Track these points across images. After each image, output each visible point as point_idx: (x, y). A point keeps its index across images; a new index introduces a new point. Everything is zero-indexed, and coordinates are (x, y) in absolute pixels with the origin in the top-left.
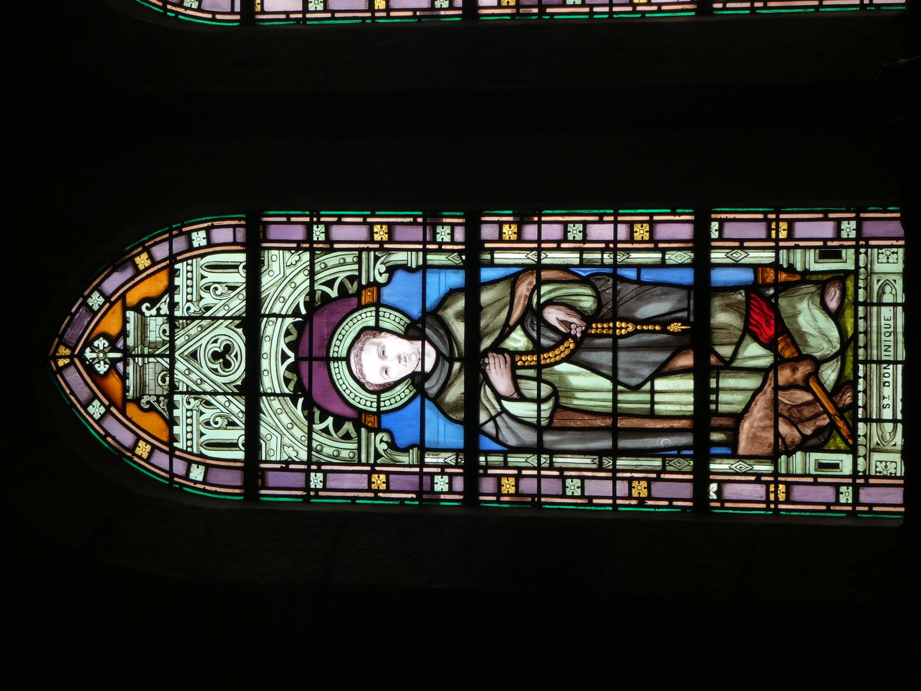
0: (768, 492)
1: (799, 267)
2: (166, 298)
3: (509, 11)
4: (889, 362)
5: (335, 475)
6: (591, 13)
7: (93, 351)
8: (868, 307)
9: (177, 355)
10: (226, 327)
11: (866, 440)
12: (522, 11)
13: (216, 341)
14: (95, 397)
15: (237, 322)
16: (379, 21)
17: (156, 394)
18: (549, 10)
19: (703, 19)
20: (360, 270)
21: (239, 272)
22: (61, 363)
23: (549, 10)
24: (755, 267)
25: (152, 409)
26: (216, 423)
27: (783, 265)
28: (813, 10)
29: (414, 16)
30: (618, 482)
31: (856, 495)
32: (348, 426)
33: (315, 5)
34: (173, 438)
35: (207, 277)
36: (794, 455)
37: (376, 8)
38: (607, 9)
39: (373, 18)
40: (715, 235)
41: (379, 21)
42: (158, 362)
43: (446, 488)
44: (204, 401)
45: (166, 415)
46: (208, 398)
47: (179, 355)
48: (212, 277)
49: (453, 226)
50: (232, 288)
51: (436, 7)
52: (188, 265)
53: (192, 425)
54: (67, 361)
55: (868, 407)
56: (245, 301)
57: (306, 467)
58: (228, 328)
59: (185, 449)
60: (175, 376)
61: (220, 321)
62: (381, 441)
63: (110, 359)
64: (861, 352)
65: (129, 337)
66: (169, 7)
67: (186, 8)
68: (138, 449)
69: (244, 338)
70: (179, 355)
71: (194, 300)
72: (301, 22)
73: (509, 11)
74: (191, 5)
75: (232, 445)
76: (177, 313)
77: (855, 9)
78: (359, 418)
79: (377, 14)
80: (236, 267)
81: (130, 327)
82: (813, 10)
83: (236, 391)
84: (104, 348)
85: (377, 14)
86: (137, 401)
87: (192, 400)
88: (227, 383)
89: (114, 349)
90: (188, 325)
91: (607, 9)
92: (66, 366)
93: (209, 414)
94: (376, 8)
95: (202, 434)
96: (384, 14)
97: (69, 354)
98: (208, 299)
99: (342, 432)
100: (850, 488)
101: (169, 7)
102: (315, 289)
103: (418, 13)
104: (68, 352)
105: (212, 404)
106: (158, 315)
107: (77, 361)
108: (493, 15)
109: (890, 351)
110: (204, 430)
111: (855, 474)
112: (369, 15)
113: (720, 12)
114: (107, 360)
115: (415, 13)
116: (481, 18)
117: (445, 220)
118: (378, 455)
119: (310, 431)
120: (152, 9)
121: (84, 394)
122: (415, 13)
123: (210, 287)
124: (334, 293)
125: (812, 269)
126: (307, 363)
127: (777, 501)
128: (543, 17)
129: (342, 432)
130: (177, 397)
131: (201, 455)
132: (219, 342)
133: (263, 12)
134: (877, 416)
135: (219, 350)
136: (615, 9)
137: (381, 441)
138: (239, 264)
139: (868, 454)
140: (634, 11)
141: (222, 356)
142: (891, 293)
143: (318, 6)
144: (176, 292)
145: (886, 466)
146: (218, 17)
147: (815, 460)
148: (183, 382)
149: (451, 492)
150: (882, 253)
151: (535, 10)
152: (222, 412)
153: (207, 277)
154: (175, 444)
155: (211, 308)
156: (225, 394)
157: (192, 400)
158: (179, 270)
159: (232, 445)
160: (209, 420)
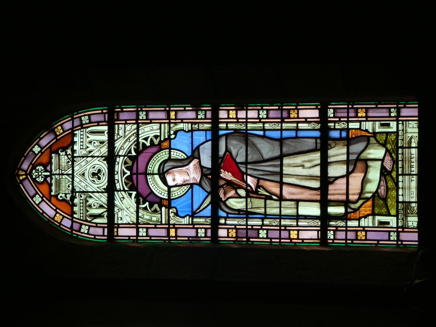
3: (232, 239)
6: (271, 242)
8: (404, 176)
9: (75, 174)
10: (98, 161)
11: (403, 142)
12: (238, 239)
13: (94, 168)
14: (37, 193)
15: (103, 158)
16: (172, 241)
18: (251, 240)
19: (323, 249)
20: (160, 132)
21: (105, 135)
22: (21, 178)
23: (251, 240)
26: (94, 206)
28: (374, 245)
29: (189, 240)
30: (348, 233)
31: (398, 236)
32: (156, 206)
33: (142, 233)
34: (73, 213)
35: (89, 147)
37: (171, 235)
38: (278, 240)
39: (169, 240)
41: (172, 241)
43: (203, 235)
44: (89, 195)
46: (91, 194)
47: (76, 174)
48: (92, 137)
49: (206, 111)
50: (102, 143)
51: (199, 236)
52: (81, 131)
53: (83, 138)
54: (24, 177)
56: (107, 149)
57: (136, 109)
58: (99, 161)
59: (79, 218)
60: (74, 184)
61: (96, 158)
64: (400, 170)
65: (53, 179)
66: (74, 232)
67: (82, 233)
69: (107, 165)
70: (76, 174)
71: (84, 148)
72: (136, 241)
73: (232, 239)
74: (84, 231)
76: (75, 155)
77: (394, 246)
78: (160, 202)
79: (171, 238)
80: (103, 132)
81: (53, 160)
82: (374, 245)
83: (103, 191)
84: (41, 170)
85: (171, 238)
87: (82, 195)
88: (99, 187)
89: (46, 171)
90: (80, 160)
91: (278, 240)
92: (24, 179)
94: (171, 235)
96: (174, 239)
98: (91, 147)
99: (153, 209)
100: (396, 233)
101: (74, 232)
102: (139, 141)
103: (190, 239)
104: (24, 173)
105: (92, 197)
108: (225, 241)
111: (398, 227)
112: (167, 238)
113: (331, 244)
115: (189, 239)
116: (220, 242)
117: (202, 108)
119: (138, 208)
120: (66, 232)
121: (32, 192)
122: (189, 239)
123: (92, 142)
124: (148, 144)
128: (248, 243)
129: (153, 209)
132: (95, 168)
133: (118, 236)
135: (95, 172)
136: (282, 241)
138: (104, 131)
140: (291, 242)
141: (96, 175)
142: (414, 142)
143: (143, 234)
144: (75, 144)
146: (97, 237)
147: (379, 128)
148: (78, 187)
149: (206, 236)
150: (411, 124)
151: (245, 239)
152: (97, 200)
153: (89, 147)
154: (75, 216)
155: (92, 151)
156: (98, 192)
157: (82, 195)
158: (77, 134)
159: (100, 216)
160: (91, 204)
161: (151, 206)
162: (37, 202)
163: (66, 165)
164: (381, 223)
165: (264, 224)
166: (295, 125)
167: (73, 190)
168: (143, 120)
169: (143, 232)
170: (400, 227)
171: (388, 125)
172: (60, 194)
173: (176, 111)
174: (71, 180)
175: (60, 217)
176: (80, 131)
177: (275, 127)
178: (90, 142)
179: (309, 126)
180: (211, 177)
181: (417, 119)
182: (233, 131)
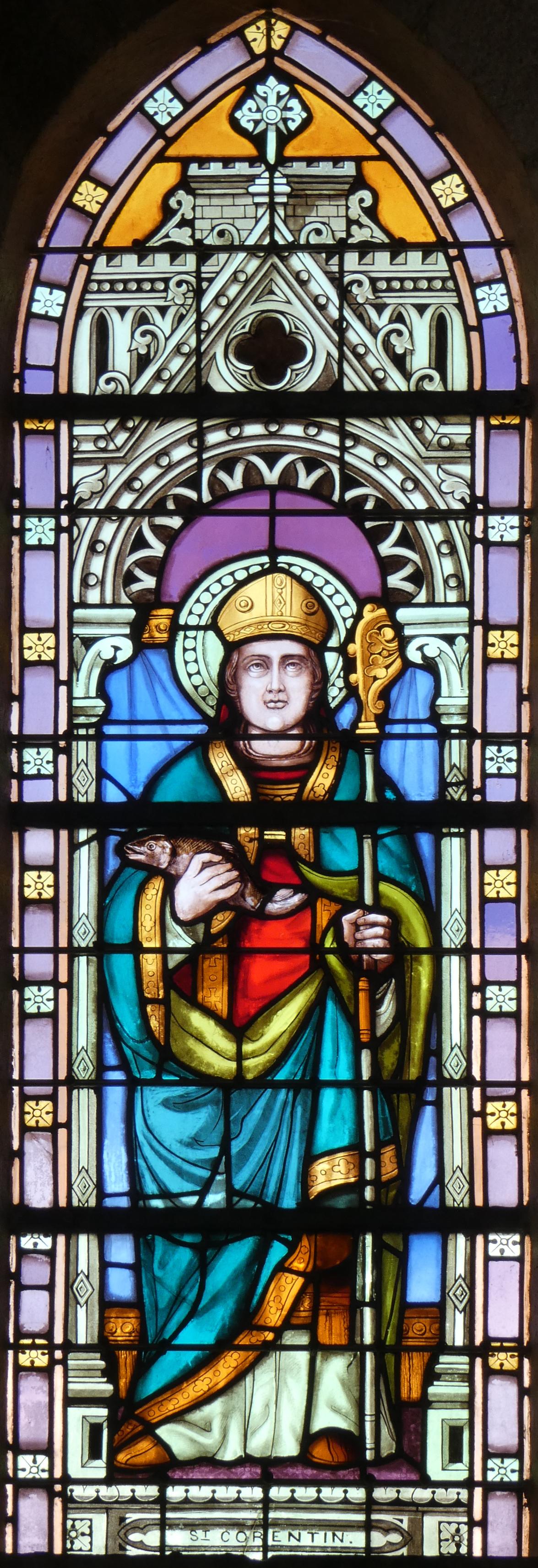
0: (33, 1336)
4: (265, 1540)
5: (53, 465)
25: (167, 212)
27: (439, 1363)
30: (50, 957)
34: (113, 253)
45: (155, 242)
54: (259, 47)
55: (187, 1506)
62: (117, 649)
63: (264, 133)
68: (91, 186)
75: (101, 364)
86: (185, 183)
89: (284, 139)
93: (164, 324)
95: (122, 311)
97: (273, 46)
100: (45, 1475)
104: (277, 44)
106: (350, 222)
107: (260, 64)
109: (289, 1540)
110: (130, 315)
114: (261, 127)
118: (88, 642)
123: (403, 322)
127: (19, 1349)
130: (191, 260)
131: (81, 311)
137: (117, 649)
143: (494, 1001)
145: (83, 1534)
154: (102, 260)
159: (101, 364)
161: (146, 565)
165: (76, 959)
167: (203, 252)
168: (486, 644)
169: (39, 999)
171: (455, 1456)
172: (191, 198)
173: (517, 1374)
174: (251, 241)
176: (448, 274)
177: (454, 1298)
178: (399, 318)
179: (454, 1172)
181: (479, 1202)
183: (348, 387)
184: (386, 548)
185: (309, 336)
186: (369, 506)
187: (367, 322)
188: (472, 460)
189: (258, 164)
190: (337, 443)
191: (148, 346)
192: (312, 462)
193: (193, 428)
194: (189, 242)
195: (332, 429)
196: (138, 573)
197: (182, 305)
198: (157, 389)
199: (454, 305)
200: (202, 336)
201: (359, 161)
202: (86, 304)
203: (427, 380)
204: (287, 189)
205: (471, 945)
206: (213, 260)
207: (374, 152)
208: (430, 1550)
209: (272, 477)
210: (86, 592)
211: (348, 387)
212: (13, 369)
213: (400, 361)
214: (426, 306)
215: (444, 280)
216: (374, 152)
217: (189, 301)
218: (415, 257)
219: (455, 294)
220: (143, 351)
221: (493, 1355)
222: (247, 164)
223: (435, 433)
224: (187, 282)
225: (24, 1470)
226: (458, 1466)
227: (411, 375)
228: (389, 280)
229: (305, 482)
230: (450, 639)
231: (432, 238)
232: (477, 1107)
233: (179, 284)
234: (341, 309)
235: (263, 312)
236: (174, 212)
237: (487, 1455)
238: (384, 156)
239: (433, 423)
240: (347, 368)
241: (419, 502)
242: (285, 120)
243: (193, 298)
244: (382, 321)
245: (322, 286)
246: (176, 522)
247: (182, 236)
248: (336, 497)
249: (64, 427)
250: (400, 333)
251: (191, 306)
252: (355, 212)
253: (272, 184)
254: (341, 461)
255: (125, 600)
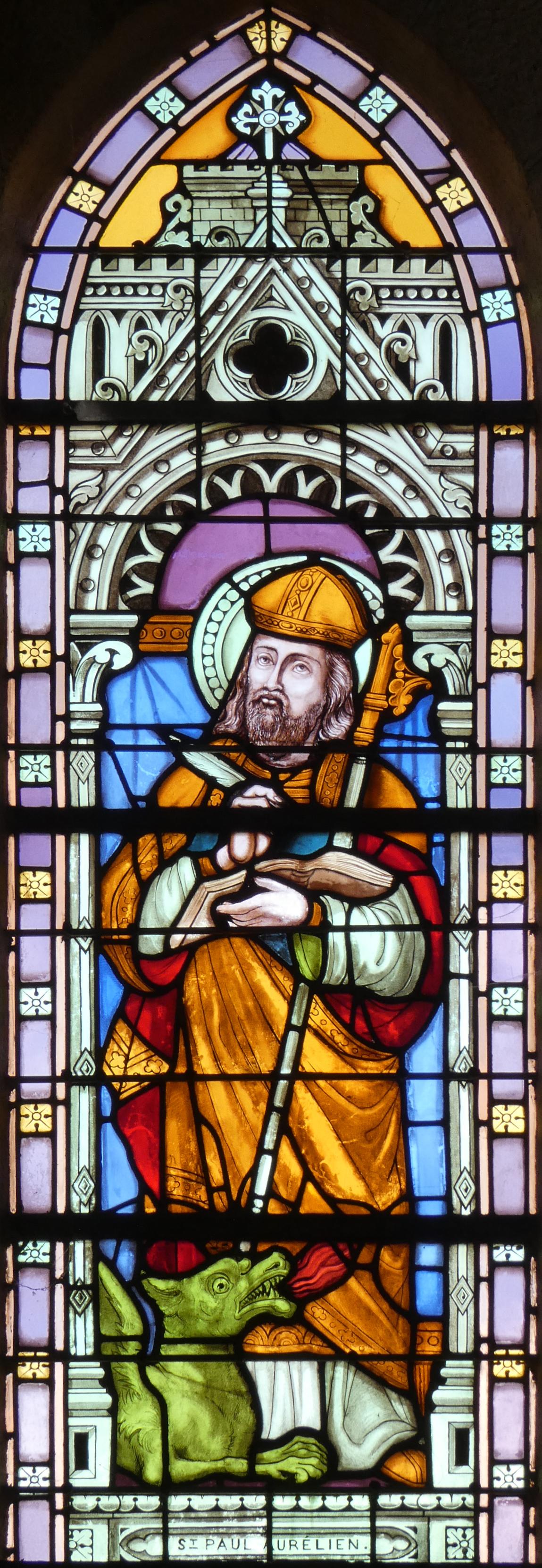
1: (438, 1395)
2: (383, 242)
7: (276, 100)
14: (190, 104)
17: (194, 223)
24: (443, 1320)
25: (167, 217)
31: (36, 1494)
36: (104, 1390)
40: (500, 1255)
42: (256, 226)
54: (260, 47)
59: (90, 280)
62: (113, 652)
89: (281, 140)
97: (274, 48)
100: (46, 1484)
104: (278, 46)
107: (262, 64)
111: (69, 1491)
125: (434, 1418)
126: (261, 514)
130: (189, 264)
131: (77, 314)
134: (174, 1528)
137: (113, 652)
139: (101, 1515)
147: (449, 1423)
150: (464, 1536)
154: (97, 263)
161: (144, 571)
162: (151, 105)
163: (309, 225)
164: (82, 1440)
166: (465, 969)
170: (67, 1500)
171: (461, 1458)
172: (188, 201)
175: (90, 203)
176: (452, 283)
179: (460, 1052)
180: (10, 1562)
182: (442, 883)
183: (350, 396)
184: (387, 555)
185: (310, 345)
186: (371, 513)
187: (370, 330)
188: (475, 470)
189: (257, 167)
190: (338, 452)
191: (147, 353)
192: (312, 469)
193: (193, 434)
194: (187, 245)
195: (332, 437)
196: (135, 579)
197: (181, 311)
198: (156, 396)
199: (460, 314)
200: (202, 342)
201: (362, 165)
202: (82, 307)
203: (431, 391)
204: (287, 193)
205: (478, 1070)
206: (212, 265)
207: (378, 156)
208: (437, 1556)
209: (271, 485)
210: (84, 597)
211: (350, 396)
212: (6, 1352)
213: (402, 370)
214: (429, 315)
215: (450, 290)
216: (378, 156)
217: (188, 307)
218: (418, 265)
219: (459, 303)
220: (141, 358)
221: (499, 1363)
222: (245, 167)
223: (439, 442)
224: (185, 288)
225: (25, 1479)
226: (464, 1469)
227: (415, 385)
228: (392, 289)
229: (305, 490)
230: (455, 648)
231: (435, 242)
232: (483, 1115)
233: (177, 289)
234: (343, 317)
235: (260, 320)
236: (173, 215)
237: (493, 1462)
238: (386, 160)
239: (436, 432)
240: (349, 377)
241: (421, 511)
242: (283, 124)
243: (192, 303)
244: (384, 331)
245: (323, 292)
246: (175, 528)
247: (181, 240)
248: (337, 505)
249: (60, 434)
250: (404, 342)
251: (189, 311)
252: (358, 217)
253: (270, 188)
254: (343, 471)
255: (122, 606)
